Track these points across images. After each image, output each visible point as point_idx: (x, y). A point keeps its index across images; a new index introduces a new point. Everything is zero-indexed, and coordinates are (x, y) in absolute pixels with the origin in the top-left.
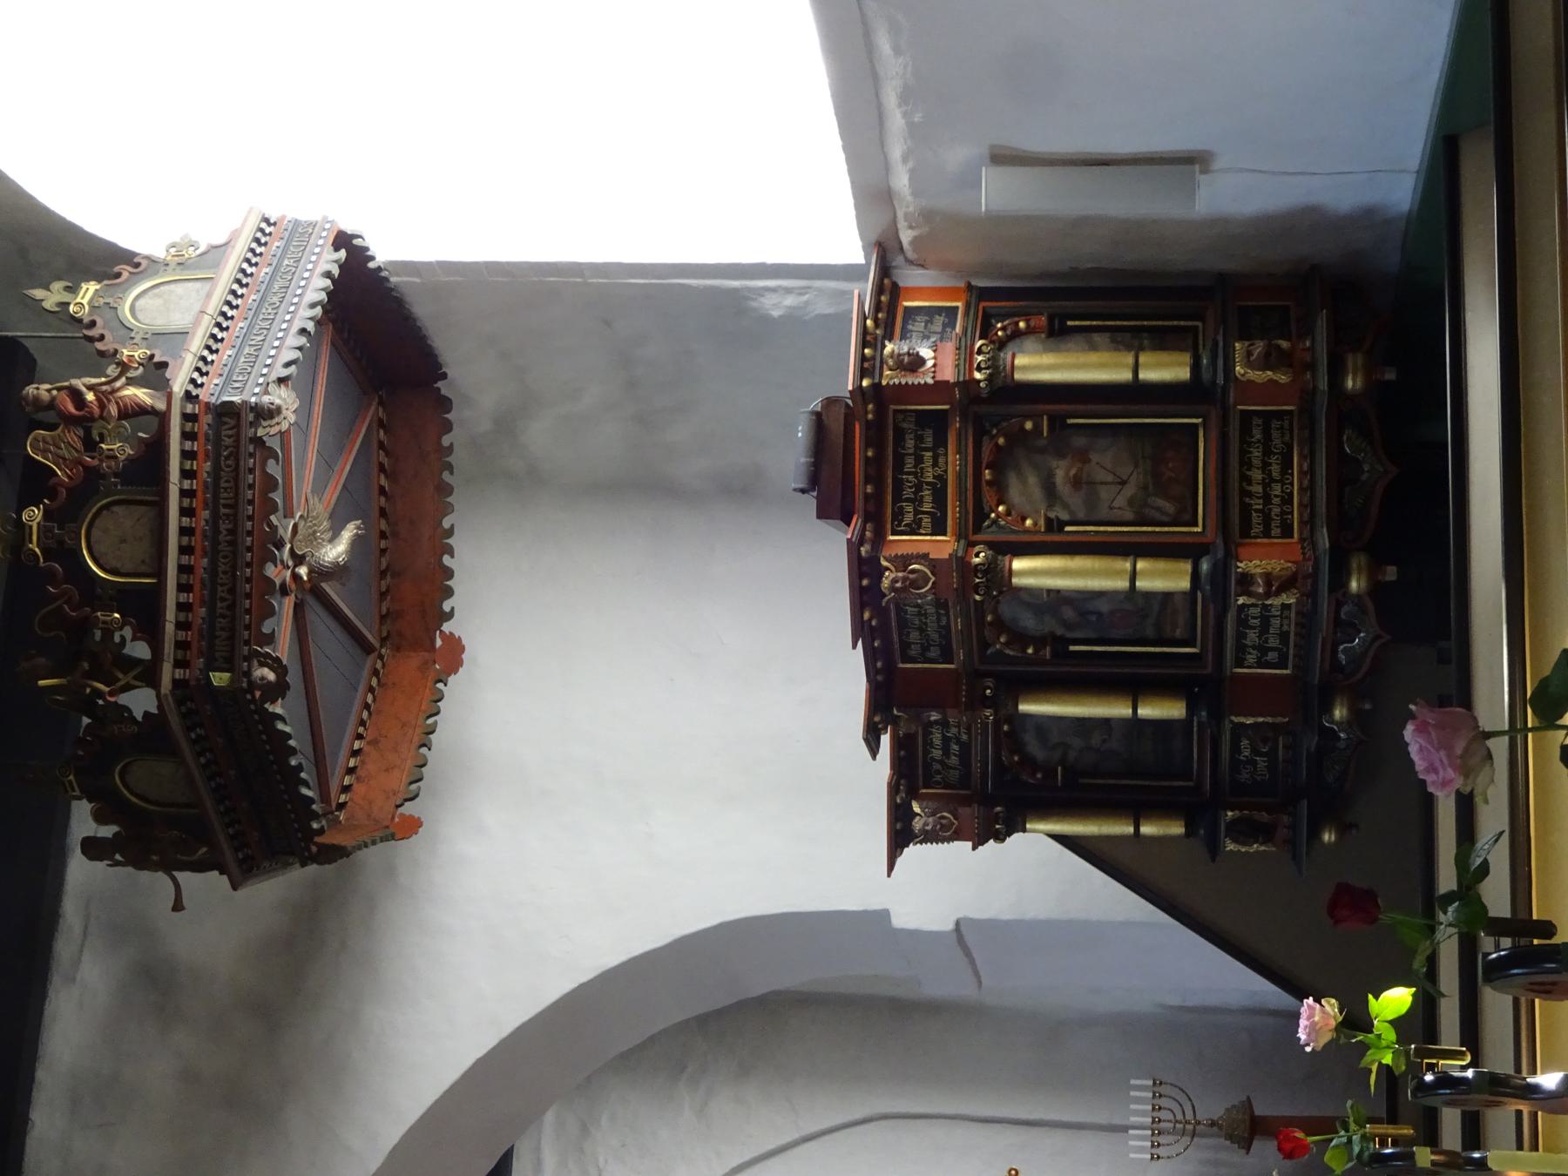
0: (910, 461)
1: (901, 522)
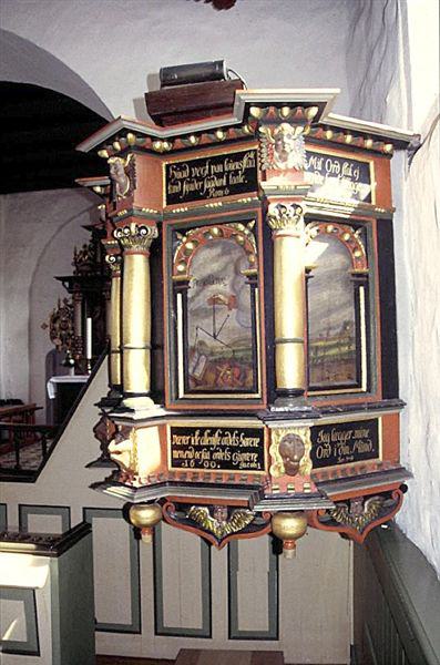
0: (219, 169)
1: (175, 170)
